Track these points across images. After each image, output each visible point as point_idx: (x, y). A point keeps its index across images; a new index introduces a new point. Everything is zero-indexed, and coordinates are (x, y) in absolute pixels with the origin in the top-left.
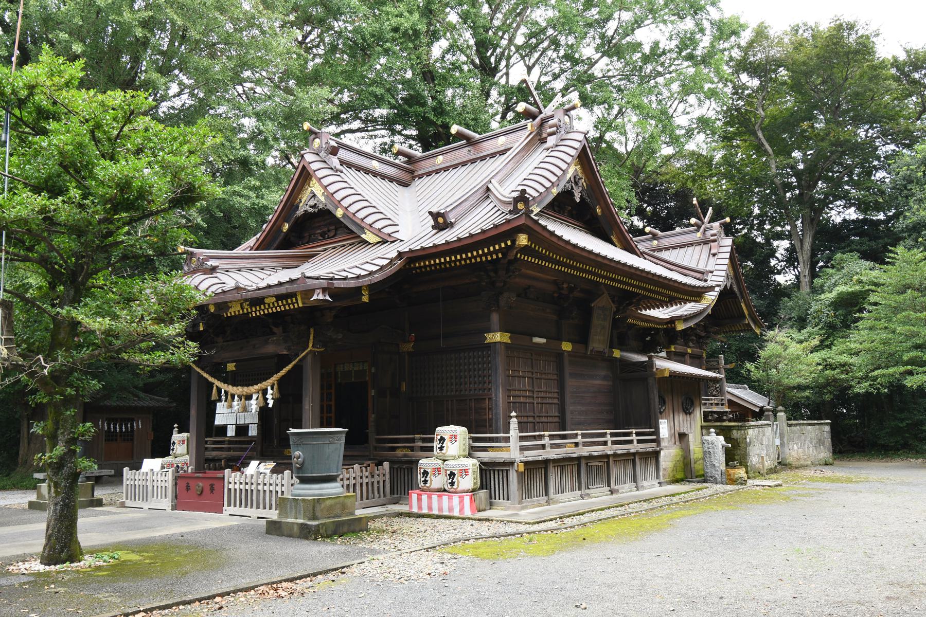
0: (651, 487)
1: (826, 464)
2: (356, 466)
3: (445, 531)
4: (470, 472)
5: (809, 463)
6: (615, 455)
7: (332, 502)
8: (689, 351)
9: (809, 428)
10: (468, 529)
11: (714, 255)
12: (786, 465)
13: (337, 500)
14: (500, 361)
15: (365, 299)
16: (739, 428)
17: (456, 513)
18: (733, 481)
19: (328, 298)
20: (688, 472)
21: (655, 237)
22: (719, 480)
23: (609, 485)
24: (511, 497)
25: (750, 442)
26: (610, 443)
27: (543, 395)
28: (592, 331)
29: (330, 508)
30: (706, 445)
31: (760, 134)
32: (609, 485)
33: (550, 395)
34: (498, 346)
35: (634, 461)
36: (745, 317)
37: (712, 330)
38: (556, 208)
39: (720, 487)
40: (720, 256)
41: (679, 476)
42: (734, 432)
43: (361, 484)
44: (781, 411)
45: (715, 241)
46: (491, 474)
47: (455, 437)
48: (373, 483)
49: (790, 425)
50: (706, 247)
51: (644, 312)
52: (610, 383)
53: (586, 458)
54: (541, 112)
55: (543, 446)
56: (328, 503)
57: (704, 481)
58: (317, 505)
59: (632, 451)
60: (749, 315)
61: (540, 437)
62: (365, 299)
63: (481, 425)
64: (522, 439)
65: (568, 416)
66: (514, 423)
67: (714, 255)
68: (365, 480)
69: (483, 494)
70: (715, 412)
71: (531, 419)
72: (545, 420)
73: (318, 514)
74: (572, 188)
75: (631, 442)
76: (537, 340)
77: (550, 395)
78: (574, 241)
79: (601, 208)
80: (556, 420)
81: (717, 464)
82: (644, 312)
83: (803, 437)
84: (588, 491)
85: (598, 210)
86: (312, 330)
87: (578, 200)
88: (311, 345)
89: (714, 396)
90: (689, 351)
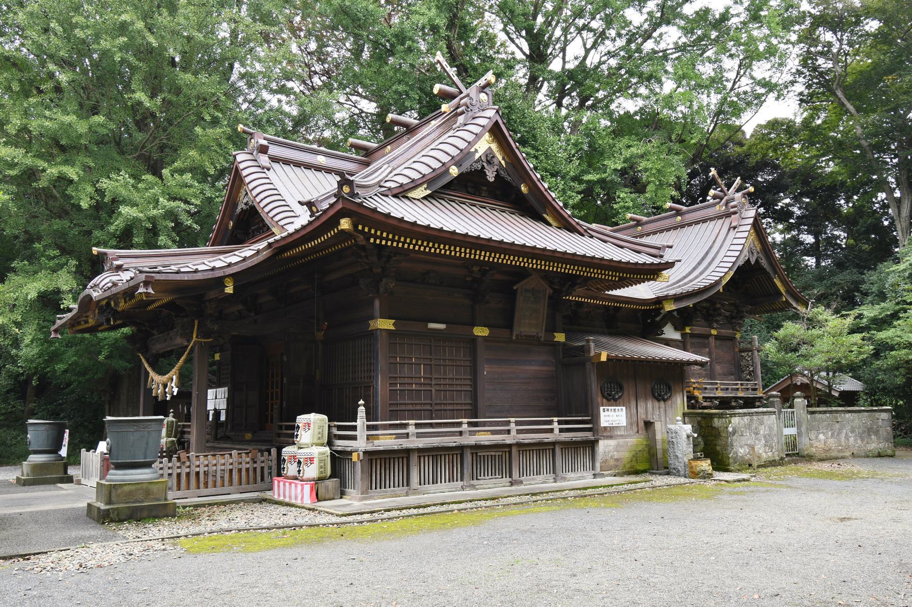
0: (579, 478)
1: (880, 456)
2: (234, 452)
3: (292, 517)
4: (316, 461)
5: (848, 454)
6: (519, 445)
7: (133, 488)
8: (714, 332)
9: (848, 415)
10: (308, 518)
11: (735, 228)
12: (803, 457)
13: (139, 486)
14: (382, 348)
15: (229, 290)
16: (720, 416)
17: (299, 502)
18: (695, 474)
19: (150, 291)
20: (651, 461)
21: (679, 213)
22: (682, 473)
23: (511, 476)
24: (356, 487)
25: (734, 432)
26: (513, 433)
27: (447, 382)
28: (517, 314)
29: (130, 493)
30: (670, 435)
31: (839, 93)
32: (511, 476)
33: (459, 382)
34: (379, 332)
35: (554, 451)
36: (782, 294)
37: (744, 309)
38: (470, 190)
39: (682, 480)
40: (741, 228)
41: (640, 467)
42: (716, 420)
43: (240, 471)
44: (799, 397)
45: (735, 213)
46: (339, 462)
47: (309, 425)
48: (255, 469)
49: (813, 413)
50: (728, 221)
51: (610, 292)
52: (554, 369)
53: (472, 447)
54: (461, 92)
55: (461, 433)
56: (126, 488)
57: (668, 474)
58: (113, 490)
59: (508, 442)
60: (787, 291)
61: (405, 426)
62: (229, 290)
63: (340, 413)
64: (369, 428)
65: (481, 404)
66: (361, 411)
67: (735, 228)
68: (244, 466)
69: (332, 483)
70: (741, 398)
71: (429, 407)
72: (449, 407)
73: (114, 499)
74: (483, 167)
75: (552, 431)
76: (432, 326)
77: (459, 382)
78: (409, 218)
79: (527, 185)
80: (469, 407)
81: (680, 456)
82: (610, 292)
83: (837, 426)
84: (475, 482)
85: (523, 188)
86: (196, 322)
87: (492, 179)
88: (194, 336)
89: (748, 380)
90: (714, 332)
